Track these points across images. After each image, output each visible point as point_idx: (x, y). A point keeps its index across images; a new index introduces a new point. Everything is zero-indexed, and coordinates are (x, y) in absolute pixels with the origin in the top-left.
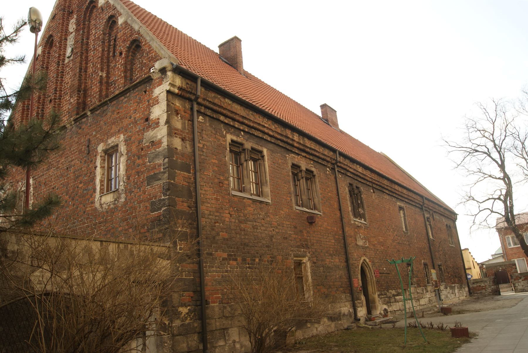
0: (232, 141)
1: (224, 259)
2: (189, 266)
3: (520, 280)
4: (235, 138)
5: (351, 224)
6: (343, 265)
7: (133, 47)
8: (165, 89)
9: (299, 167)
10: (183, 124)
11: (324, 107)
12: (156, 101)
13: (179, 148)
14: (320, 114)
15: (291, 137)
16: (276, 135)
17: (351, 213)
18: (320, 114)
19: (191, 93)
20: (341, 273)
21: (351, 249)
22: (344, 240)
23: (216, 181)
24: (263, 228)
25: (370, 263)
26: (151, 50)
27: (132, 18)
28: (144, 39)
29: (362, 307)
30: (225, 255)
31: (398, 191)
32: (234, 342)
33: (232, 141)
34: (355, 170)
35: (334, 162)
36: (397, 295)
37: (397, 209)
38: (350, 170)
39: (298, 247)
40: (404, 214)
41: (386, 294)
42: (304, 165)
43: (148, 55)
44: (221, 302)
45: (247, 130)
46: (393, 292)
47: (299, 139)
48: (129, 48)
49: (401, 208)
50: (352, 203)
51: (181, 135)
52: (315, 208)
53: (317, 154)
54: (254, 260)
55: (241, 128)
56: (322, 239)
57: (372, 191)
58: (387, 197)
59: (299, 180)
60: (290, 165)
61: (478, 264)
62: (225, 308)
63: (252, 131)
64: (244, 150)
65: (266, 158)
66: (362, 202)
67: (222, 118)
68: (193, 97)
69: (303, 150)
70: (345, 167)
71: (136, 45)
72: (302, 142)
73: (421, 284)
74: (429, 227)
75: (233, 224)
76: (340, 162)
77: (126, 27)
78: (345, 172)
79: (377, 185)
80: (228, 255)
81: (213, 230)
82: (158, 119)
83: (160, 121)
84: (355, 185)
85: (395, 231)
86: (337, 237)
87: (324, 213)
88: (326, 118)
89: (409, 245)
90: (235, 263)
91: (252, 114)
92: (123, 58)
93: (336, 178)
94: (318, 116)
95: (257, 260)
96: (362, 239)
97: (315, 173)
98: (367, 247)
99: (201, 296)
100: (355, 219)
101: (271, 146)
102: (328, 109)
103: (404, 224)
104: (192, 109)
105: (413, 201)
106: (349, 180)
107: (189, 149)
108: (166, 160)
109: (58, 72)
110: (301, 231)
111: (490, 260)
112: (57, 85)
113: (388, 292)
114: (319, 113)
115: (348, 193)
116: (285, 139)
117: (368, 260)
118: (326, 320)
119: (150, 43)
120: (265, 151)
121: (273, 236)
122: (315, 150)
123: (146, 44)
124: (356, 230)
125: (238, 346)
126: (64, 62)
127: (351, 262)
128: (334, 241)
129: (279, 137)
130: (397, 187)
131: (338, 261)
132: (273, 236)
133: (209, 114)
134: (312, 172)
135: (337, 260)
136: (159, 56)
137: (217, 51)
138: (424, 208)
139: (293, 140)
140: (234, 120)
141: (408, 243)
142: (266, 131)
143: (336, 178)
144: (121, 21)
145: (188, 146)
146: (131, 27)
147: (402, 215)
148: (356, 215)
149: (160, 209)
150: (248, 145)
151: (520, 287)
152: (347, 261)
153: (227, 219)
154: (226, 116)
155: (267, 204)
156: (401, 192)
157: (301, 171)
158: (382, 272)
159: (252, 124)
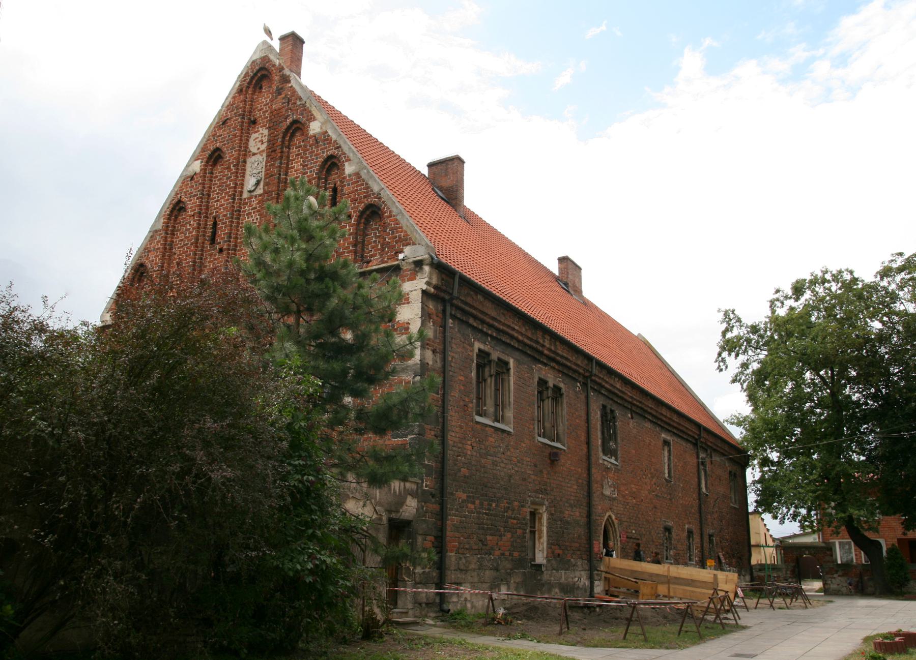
0: (480, 350)
1: (463, 501)
2: (434, 507)
3: (835, 576)
4: (482, 347)
5: (599, 465)
6: (583, 521)
7: (368, 213)
8: (419, 287)
9: (546, 382)
10: (435, 331)
11: (564, 261)
12: (403, 299)
13: (431, 363)
14: (556, 272)
15: (541, 341)
16: (526, 341)
17: (600, 449)
18: (556, 272)
19: (445, 291)
20: (581, 531)
21: (596, 499)
23: (462, 403)
24: (502, 465)
25: (616, 522)
26: (397, 228)
27: (368, 172)
28: (388, 208)
29: (599, 580)
30: (464, 496)
31: (666, 417)
32: (466, 600)
33: (480, 350)
34: (611, 385)
35: (587, 374)
37: (660, 443)
38: (607, 386)
39: (536, 491)
40: (669, 452)
42: (552, 379)
43: (393, 233)
44: (457, 552)
45: (494, 334)
47: (550, 344)
48: (362, 213)
49: (666, 443)
50: (603, 433)
52: (558, 440)
53: (569, 364)
54: (491, 505)
55: (490, 332)
56: (563, 484)
58: (648, 425)
59: (543, 401)
60: (536, 380)
61: (774, 540)
62: (460, 559)
63: (501, 338)
64: (490, 362)
65: (512, 371)
66: (615, 433)
67: (471, 321)
68: (447, 297)
69: (551, 361)
70: (600, 381)
71: (373, 212)
72: (553, 348)
73: (681, 561)
74: (702, 473)
75: (474, 458)
76: (595, 375)
77: (358, 182)
78: (599, 388)
79: (638, 406)
80: (468, 497)
81: (455, 464)
82: (408, 323)
83: (410, 326)
84: (609, 407)
85: (653, 477)
87: (569, 448)
88: (565, 280)
89: (670, 500)
90: (472, 507)
92: (353, 225)
93: (587, 397)
94: (553, 275)
95: (494, 505)
96: (610, 487)
97: (563, 391)
98: (614, 499)
99: (442, 543)
100: (605, 458)
101: (517, 354)
102: (570, 266)
103: (666, 467)
104: (444, 311)
105: (684, 432)
106: (602, 401)
107: (439, 364)
108: (418, 378)
109: (233, 211)
110: (541, 471)
111: (795, 536)
112: (231, 230)
114: (555, 268)
115: (599, 419)
116: (534, 345)
117: (613, 517)
118: (557, 590)
119: (398, 217)
120: (511, 361)
121: (511, 476)
122: (567, 359)
123: (390, 216)
125: (469, 605)
126: (241, 195)
127: (594, 517)
128: (575, 487)
129: (528, 342)
130: (664, 411)
131: (577, 514)
132: (511, 476)
133: (459, 316)
134: (560, 389)
135: (577, 514)
136: (410, 239)
137: (425, 171)
138: (699, 444)
139: (543, 346)
140: (483, 322)
142: (516, 335)
143: (587, 397)
144: (349, 169)
145: (438, 360)
146: (367, 184)
147: (666, 454)
148: (607, 451)
149: (406, 436)
150: (495, 356)
151: (834, 586)
152: (589, 515)
153: (469, 453)
154: (475, 318)
155: (509, 433)
156: (670, 419)
157: (547, 388)
158: (630, 535)
159: (501, 327)
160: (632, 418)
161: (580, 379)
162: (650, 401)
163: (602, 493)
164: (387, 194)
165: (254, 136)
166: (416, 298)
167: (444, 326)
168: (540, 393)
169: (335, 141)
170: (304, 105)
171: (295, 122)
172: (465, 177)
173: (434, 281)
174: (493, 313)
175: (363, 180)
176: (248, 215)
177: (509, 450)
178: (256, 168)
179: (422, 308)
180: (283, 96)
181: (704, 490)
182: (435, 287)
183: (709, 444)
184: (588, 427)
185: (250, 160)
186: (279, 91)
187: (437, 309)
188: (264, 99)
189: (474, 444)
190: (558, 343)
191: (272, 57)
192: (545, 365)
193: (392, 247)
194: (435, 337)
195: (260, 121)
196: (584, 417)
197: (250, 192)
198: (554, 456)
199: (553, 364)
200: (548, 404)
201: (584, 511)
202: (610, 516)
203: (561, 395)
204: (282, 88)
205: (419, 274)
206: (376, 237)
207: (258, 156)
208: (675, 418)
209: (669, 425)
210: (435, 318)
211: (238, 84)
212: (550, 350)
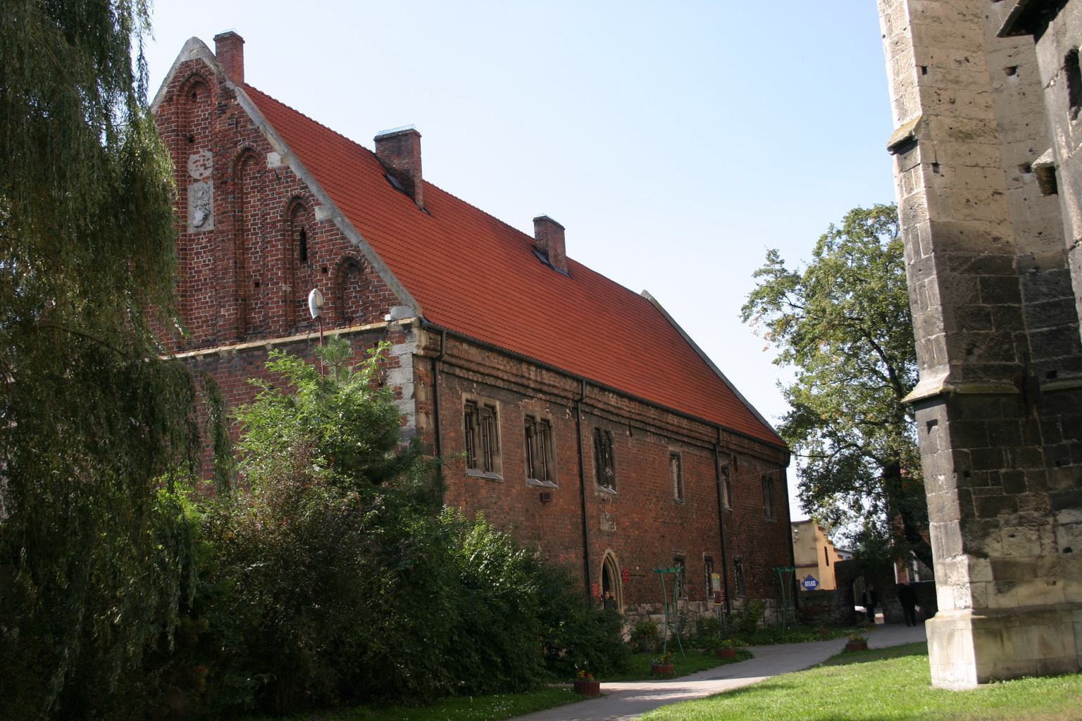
0: (467, 401)
5: (594, 498)
6: (580, 562)
8: (409, 351)
9: (533, 418)
10: (426, 393)
11: (541, 222)
13: (425, 426)
15: (527, 375)
17: (595, 479)
21: (592, 538)
22: (584, 524)
24: (495, 516)
25: (616, 560)
28: (369, 263)
33: (467, 401)
36: (654, 613)
38: (600, 405)
40: (679, 466)
41: (636, 610)
42: (538, 409)
43: (376, 291)
45: (480, 380)
46: (648, 607)
47: (536, 376)
49: (674, 456)
50: (597, 459)
51: (425, 408)
52: (548, 477)
57: (628, 432)
58: (651, 439)
60: (523, 418)
66: (611, 457)
67: (458, 371)
72: (539, 379)
73: (697, 596)
79: (637, 420)
83: (403, 391)
85: (658, 501)
86: (574, 520)
91: (488, 357)
92: (330, 279)
93: (578, 424)
96: (608, 520)
97: (552, 423)
107: (432, 426)
113: (640, 606)
114: (530, 231)
115: (593, 445)
117: (613, 555)
120: (498, 404)
124: (601, 506)
127: (591, 557)
128: (569, 527)
129: (513, 379)
134: (548, 421)
137: (372, 147)
141: (680, 522)
143: (578, 424)
146: (342, 234)
147: (675, 469)
148: (603, 480)
152: (586, 556)
154: (461, 368)
160: (631, 436)
161: (570, 405)
162: (653, 411)
163: (599, 529)
164: (365, 248)
165: (193, 157)
166: (407, 360)
167: (434, 386)
168: (528, 430)
169: (301, 180)
170: (257, 130)
171: (247, 149)
172: (422, 156)
173: (423, 344)
174: (478, 359)
175: (338, 229)
176: (196, 254)
177: (500, 498)
178: (201, 198)
179: (414, 373)
180: (228, 115)
181: (727, 506)
182: (425, 348)
183: (732, 447)
184: (580, 458)
185: (193, 188)
186: (223, 109)
187: (426, 369)
188: (201, 112)
189: (468, 500)
190: (544, 372)
191: (207, 62)
192: (532, 398)
193: (376, 306)
194: (427, 399)
195: (198, 139)
196: (576, 447)
197: (197, 227)
198: (545, 497)
199: (540, 395)
200: (537, 440)
201: (580, 551)
202: (609, 554)
203: (550, 427)
204: (226, 106)
205: (409, 338)
206: (356, 292)
207: (201, 184)
208: (685, 423)
209: (677, 433)
210: (425, 379)
211: (166, 89)
212: (536, 381)
